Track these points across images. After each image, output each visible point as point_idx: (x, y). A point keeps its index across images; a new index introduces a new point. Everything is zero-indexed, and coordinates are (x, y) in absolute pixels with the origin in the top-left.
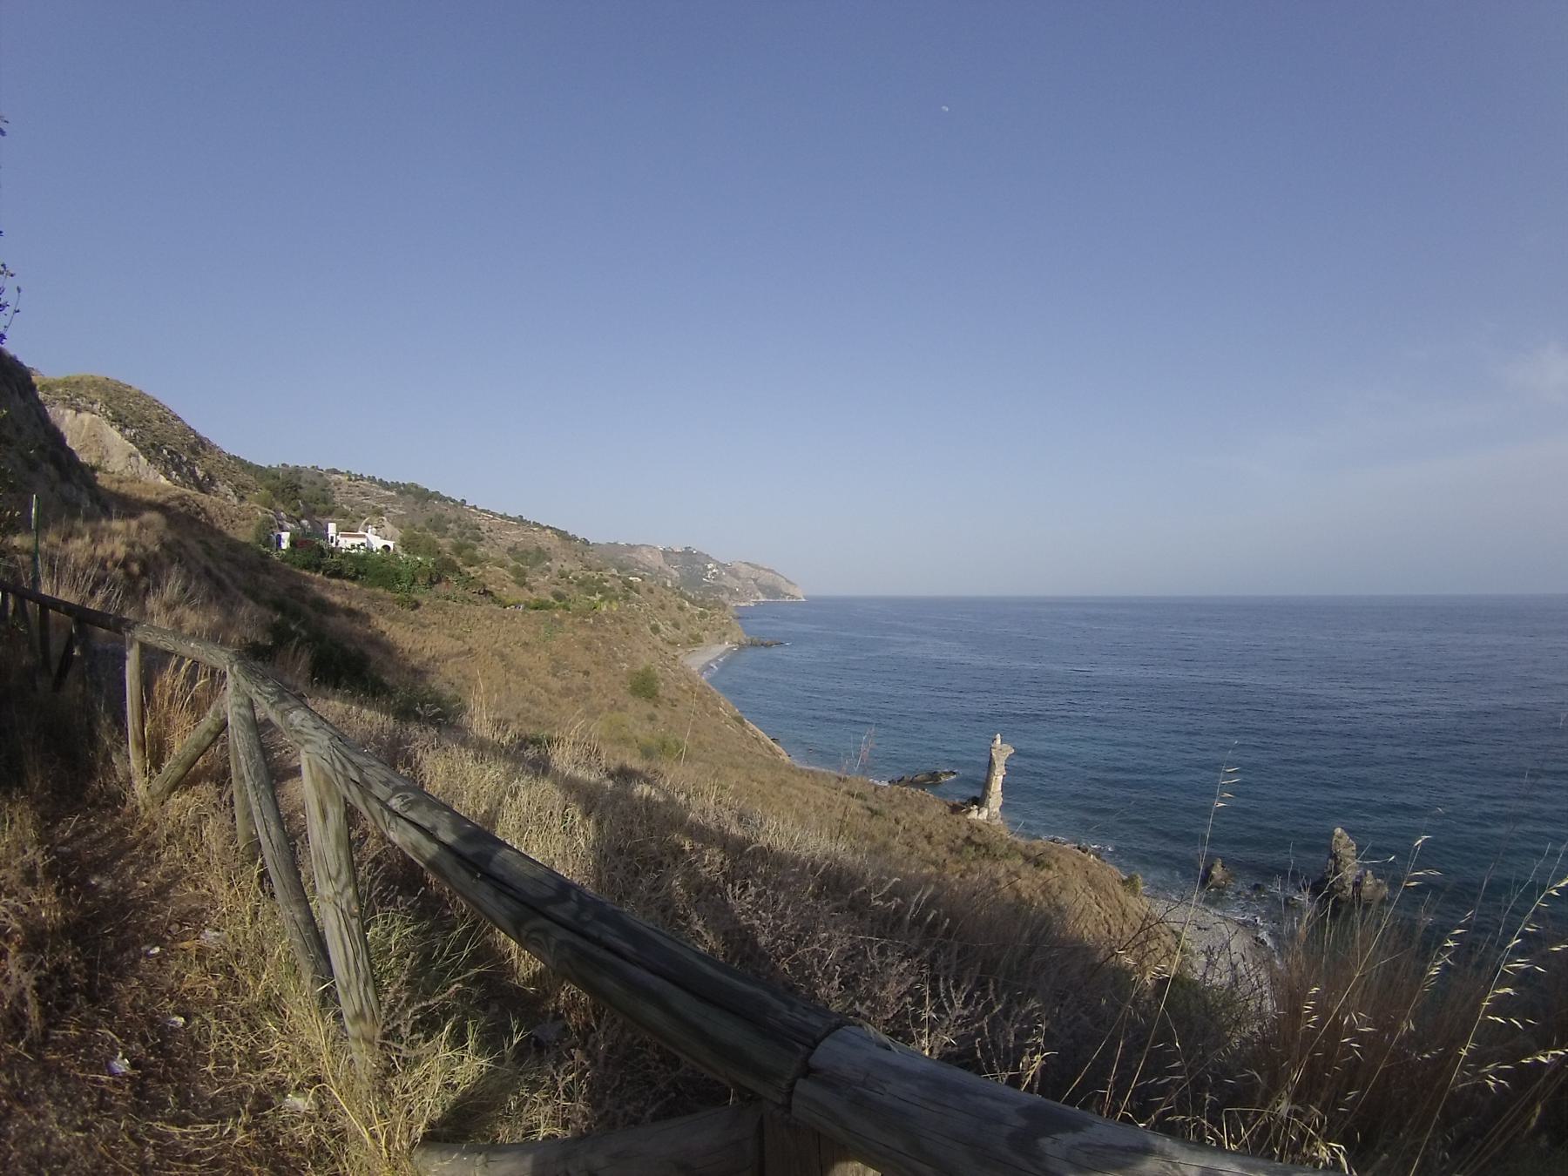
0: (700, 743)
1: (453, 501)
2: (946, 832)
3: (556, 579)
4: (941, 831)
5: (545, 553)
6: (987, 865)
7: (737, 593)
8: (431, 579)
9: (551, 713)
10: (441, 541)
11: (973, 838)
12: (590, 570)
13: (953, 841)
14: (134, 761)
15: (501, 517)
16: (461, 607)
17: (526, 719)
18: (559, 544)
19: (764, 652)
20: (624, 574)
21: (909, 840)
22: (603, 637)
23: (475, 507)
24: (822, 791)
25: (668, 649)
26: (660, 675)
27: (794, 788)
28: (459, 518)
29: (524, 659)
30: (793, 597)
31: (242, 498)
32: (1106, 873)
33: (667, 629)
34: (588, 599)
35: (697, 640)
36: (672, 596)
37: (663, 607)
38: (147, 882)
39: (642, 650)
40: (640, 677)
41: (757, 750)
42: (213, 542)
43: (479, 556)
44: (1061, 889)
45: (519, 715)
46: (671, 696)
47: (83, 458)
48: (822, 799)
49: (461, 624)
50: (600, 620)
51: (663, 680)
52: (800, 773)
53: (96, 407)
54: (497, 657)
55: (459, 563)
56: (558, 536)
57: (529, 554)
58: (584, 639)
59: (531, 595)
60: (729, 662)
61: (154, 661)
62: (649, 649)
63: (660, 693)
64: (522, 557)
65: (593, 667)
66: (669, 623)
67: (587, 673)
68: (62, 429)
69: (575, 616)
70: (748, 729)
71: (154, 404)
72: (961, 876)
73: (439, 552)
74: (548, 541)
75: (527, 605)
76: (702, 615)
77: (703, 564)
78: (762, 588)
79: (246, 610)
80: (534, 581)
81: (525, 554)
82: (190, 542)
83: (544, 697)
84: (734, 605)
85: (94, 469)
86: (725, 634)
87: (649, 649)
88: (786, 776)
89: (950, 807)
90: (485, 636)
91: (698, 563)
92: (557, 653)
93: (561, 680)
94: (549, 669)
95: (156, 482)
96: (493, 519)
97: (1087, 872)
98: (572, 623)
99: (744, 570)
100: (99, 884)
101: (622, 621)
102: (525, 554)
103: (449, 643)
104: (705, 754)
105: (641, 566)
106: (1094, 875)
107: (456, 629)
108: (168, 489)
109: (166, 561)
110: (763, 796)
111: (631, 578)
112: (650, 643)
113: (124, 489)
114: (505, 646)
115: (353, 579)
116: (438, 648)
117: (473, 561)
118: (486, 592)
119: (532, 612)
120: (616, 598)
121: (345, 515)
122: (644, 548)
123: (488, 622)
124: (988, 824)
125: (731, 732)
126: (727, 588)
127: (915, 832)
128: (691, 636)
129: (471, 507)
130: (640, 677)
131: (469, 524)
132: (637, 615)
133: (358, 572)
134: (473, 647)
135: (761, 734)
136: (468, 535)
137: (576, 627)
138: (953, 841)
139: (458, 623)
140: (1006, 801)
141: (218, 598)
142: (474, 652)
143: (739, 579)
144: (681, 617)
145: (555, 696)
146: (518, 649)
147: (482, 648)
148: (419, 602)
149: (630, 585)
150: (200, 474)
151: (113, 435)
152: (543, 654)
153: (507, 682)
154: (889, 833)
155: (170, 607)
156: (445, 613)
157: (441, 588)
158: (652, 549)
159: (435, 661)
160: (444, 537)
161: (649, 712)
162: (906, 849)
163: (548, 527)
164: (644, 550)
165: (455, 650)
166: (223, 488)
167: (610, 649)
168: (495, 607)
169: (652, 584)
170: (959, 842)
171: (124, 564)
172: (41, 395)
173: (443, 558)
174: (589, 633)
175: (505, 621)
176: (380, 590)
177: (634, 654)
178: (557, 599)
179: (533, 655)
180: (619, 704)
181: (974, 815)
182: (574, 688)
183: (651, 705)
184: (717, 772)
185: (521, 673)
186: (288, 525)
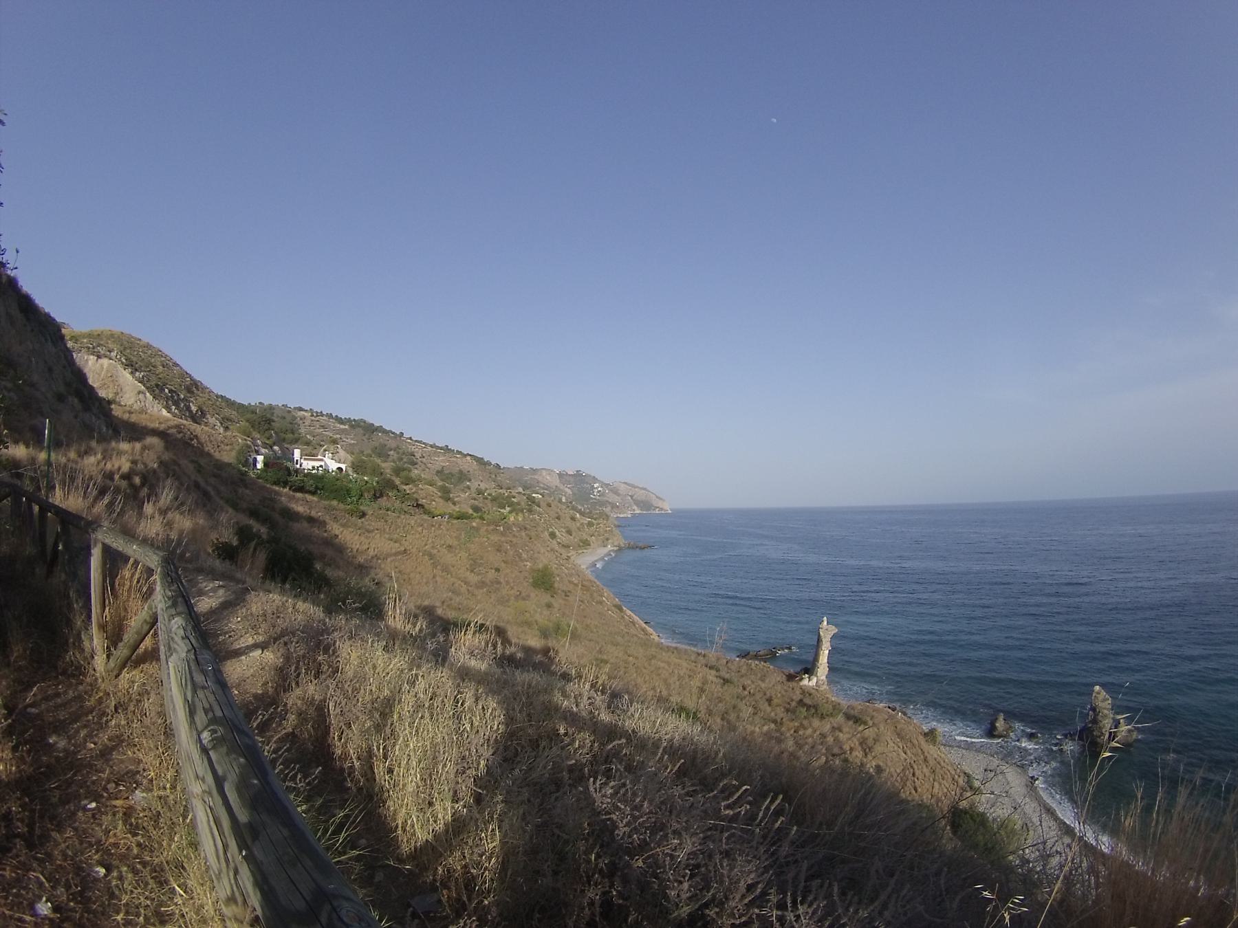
0: (587, 625)
1: (393, 433)
2: (783, 696)
3: (474, 495)
4: (779, 695)
5: (465, 475)
6: (816, 722)
7: (618, 507)
9: (469, 601)
10: (383, 465)
12: (501, 489)
13: (789, 704)
14: (96, 641)
15: (431, 446)
16: (399, 517)
18: (476, 468)
20: (528, 492)
22: (511, 541)
23: (410, 438)
24: (685, 664)
25: (563, 551)
26: (556, 572)
27: (662, 662)
29: (448, 558)
30: (662, 509)
31: (227, 428)
34: (499, 511)
35: (586, 544)
38: (95, 744)
40: (540, 574)
41: (633, 631)
42: (203, 461)
44: (875, 741)
45: (443, 602)
47: (102, 393)
48: (684, 670)
50: (508, 527)
52: (666, 649)
53: (113, 354)
54: (426, 557)
55: (397, 481)
61: (114, 560)
63: (556, 585)
65: (503, 565)
66: (564, 531)
67: (497, 570)
68: (86, 371)
69: (488, 525)
71: (158, 353)
72: (795, 732)
73: (382, 474)
74: (467, 465)
75: (451, 516)
76: (590, 524)
77: (590, 484)
78: (638, 503)
79: (228, 517)
80: (457, 497)
81: (450, 476)
82: (184, 462)
84: (615, 516)
85: (109, 402)
86: (607, 539)
88: (656, 652)
89: (787, 676)
91: (587, 483)
93: (477, 575)
94: (468, 566)
95: (159, 414)
96: (424, 447)
97: (896, 727)
98: (487, 531)
99: (622, 488)
100: (56, 743)
101: (525, 528)
102: (450, 476)
104: (591, 635)
105: (542, 485)
108: (168, 420)
109: (162, 475)
111: (534, 495)
113: (134, 418)
114: (433, 547)
115: (313, 493)
118: (418, 506)
119: (455, 521)
120: (522, 511)
121: (308, 443)
122: (544, 471)
125: (611, 616)
126: (610, 503)
127: (758, 696)
128: (581, 541)
129: (407, 438)
132: (538, 524)
133: (317, 488)
134: (408, 548)
135: (636, 618)
136: (405, 460)
137: (490, 533)
138: (789, 704)
139: (396, 530)
141: (205, 506)
142: (409, 552)
143: (619, 495)
144: (573, 526)
149: (533, 500)
150: (194, 409)
151: (126, 376)
152: (464, 554)
153: (434, 577)
154: (737, 697)
155: (163, 512)
156: (386, 521)
157: (383, 502)
158: (550, 471)
159: (378, 559)
160: (386, 461)
161: (546, 601)
164: (544, 473)
165: (394, 551)
166: (212, 420)
167: (516, 551)
168: (426, 517)
169: (550, 500)
170: (794, 704)
171: (127, 477)
172: (70, 344)
174: (500, 538)
175: (433, 529)
176: (335, 503)
178: (475, 511)
180: (523, 594)
181: (805, 682)
182: (488, 581)
183: (549, 596)
184: (600, 649)
185: (446, 569)
186: (263, 451)
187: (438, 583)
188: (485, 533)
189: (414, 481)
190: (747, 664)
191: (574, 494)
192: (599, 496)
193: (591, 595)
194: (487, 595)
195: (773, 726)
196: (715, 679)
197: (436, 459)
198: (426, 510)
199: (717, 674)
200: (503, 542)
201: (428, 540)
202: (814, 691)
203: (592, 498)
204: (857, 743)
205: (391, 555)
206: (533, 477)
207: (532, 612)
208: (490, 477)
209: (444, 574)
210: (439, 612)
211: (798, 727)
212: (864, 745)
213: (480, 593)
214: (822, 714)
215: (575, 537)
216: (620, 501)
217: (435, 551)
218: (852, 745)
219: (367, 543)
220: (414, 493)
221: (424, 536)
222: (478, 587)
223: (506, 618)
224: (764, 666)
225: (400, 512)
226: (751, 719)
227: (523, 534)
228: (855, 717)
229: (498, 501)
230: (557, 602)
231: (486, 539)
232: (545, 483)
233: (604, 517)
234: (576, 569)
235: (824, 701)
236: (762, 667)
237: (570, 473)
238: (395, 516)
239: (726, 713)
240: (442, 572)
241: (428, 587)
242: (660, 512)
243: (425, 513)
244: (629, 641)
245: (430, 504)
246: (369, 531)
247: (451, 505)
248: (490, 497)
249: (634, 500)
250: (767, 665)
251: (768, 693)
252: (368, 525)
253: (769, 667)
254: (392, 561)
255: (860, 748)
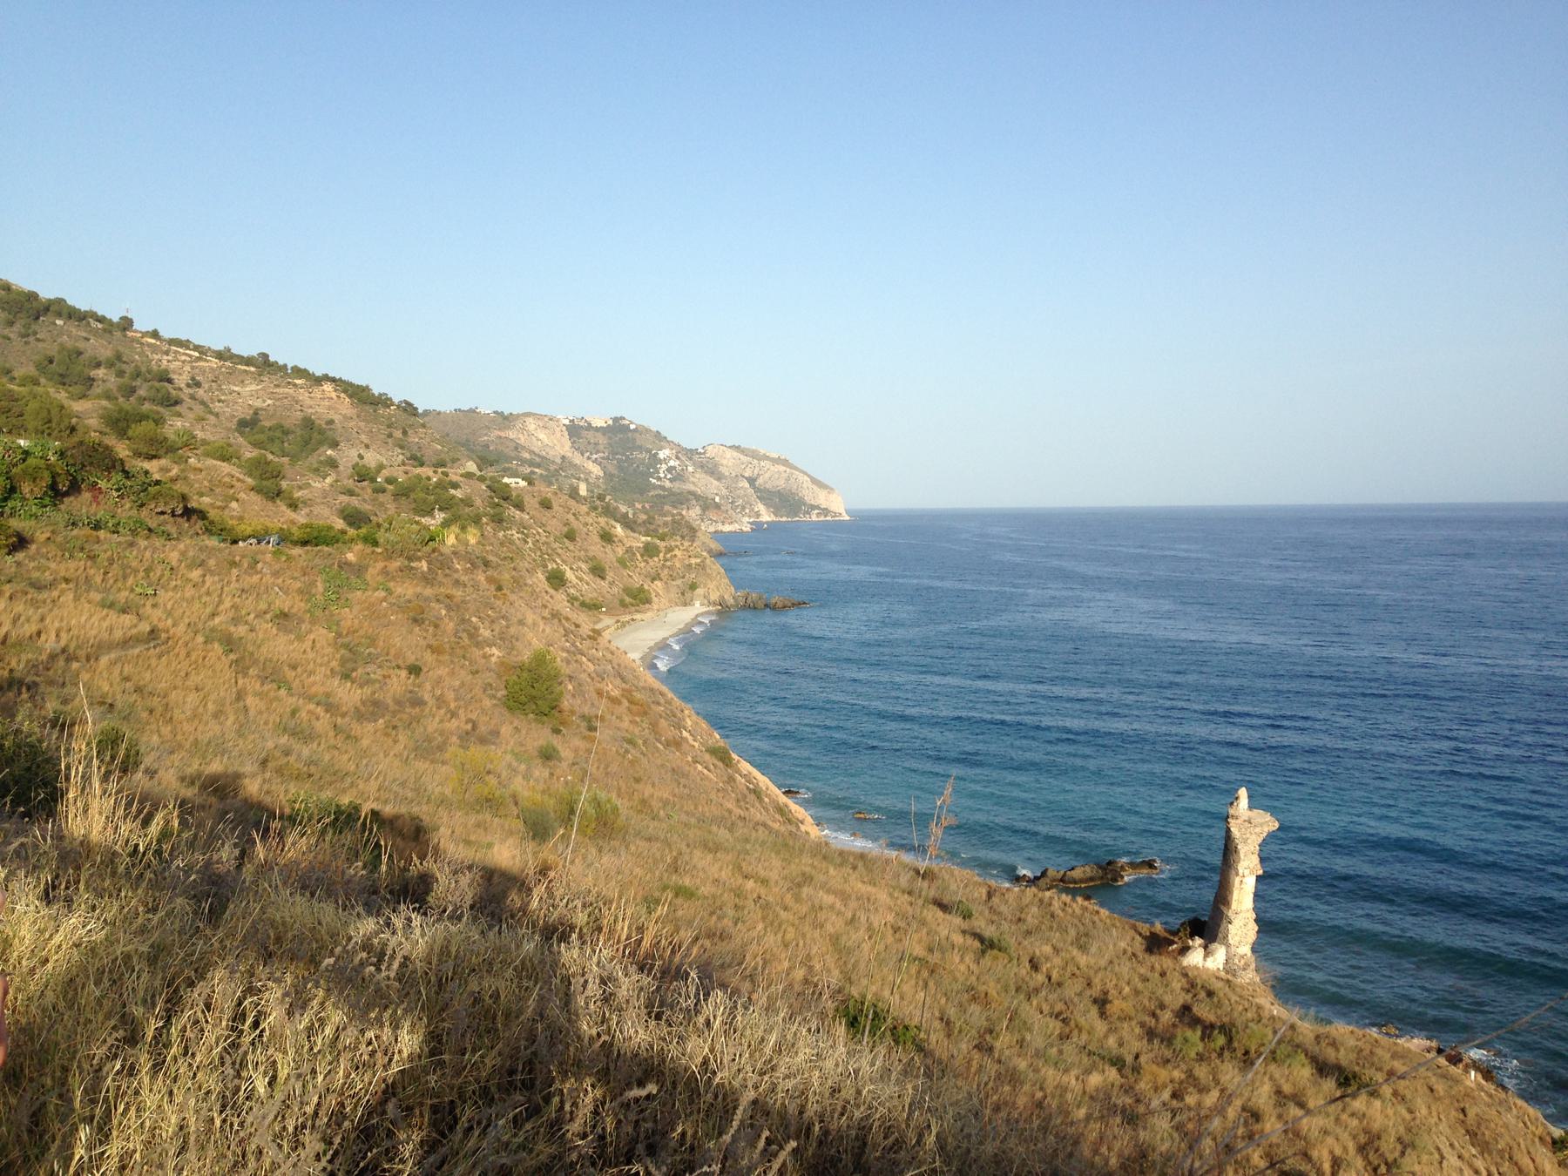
0: (644, 802)
1: (101, 319)
2: (1137, 992)
3: (350, 483)
4: (1127, 989)
5: (321, 432)
6: (1230, 1073)
7: (718, 506)
8: (53, 487)
9: (336, 753)
10: (78, 406)
11: (1195, 1009)
12: (422, 465)
13: (1154, 1015)
15: (220, 355)
16: (131, 544)
17: (279, 771)
18: (351, 412)
19: (769, 618)
21: (1059, 1007)
23: (155, 334)
25: (583, 618)
26: (566, 670)
27: (828, 891)
28: (119, 357)
29: (279, 646)
30: (826, 511)
32: (1510, 1118)
33: (581, 579)
34: (417, 523)
35: (638, 599)
36: (588, 514)
37: (570, 536)
39: (529, 621)
41: (757, 814)
43: (172, 437)
44: (1405, 1145)
45: (264, 763)
46: (586, 710)
49: (130, 581)
50: (442, 563)
51: (571, 678)
52: (838, 860)
54: (216, 645)
55: (122, 450)
56: (350, 397)
57: (286, 432)
58: (410, 601)
59: (293, 515)
60: (692, 645)
62: (543, 618)
63: (566, 704)
64: (272, 440)
65: (429, 657)
66: (583, 566)
67: (415, 670)
69: (389, 555)
70: (738, 771)
72: (1174, 1095)
73: (73, 429)
74: (325, 405)
75: (284, 538)
76: (650, 551)
77: (650, 451)
78: (766, 496)
80: (300, 488)
81: (278, 434)
83: (323, 723)
84: (712, 529)
86: (693, 587)
87: (543, 618)
88: (812, 865)
89: (1145, 938)
90: (190, 601)
91: (640, 448)
92: (353, 632)
93: (361, 687)
94: (334, 664)
96: (199, 359)
97: (1463, 1110)
98: (384, 572)
99: (729, 462)
101: (486, 564)
102: (278, 434)
103: (104, 619)
104: (652, 824)
105: (526, 455)
106: (1480, 1120)
107: (119, 590)
110: (767, 906)
111: (506, 480)
112: (545, 606)
114: (236, 621)
116: (75, 632)
117: (157, 448)
118: (188, 513)
119: (297, 551)
120: (476, 521)
122: (530, 420)
123: (195, 574)
124: (1228, 981)
126: (697, 497)
127: (1072, 989)
128: (627, 591)
129: (145, 334)
130: (525, 675)
131: (144, 369)
132: (519, 551)
134: (161, 625)
135: (763, 781)
136: (142, 392)
137: (393, 579)
138: (1154, 1015)
139: (125, 577)
140: (1213, 804)
142: (164, 635)
144: (608, 555)
145: (347, 719)
146: (266, 627)
147: (182, 628)
148: (28, 535)
149: (503, 495)
152: (322, 635)
153: (240, 696)
154: (1018, 989)
156: (92, 558)
157: (81, 504)
158: (547, 421)
159: (69, 660)
160: (84, 396)
161: (542, 742)
162: (1055, 1026)
163: (326, 378)
164: (531, 425)
165: (118, 635)
167: (463, 621)
168: (213, 542)
169: (548, 491)
170: (1167, 1017)
173: (81, 443)
174: (419, 590)
175: (235, 571)
177: (512, 630)
178: (351, 524)
179: (300, 638)
180: (483, 729)
181: (1195, 957)
184: (676, 859)
185: (273, 675)
187: (252, 712)
188: (380, 579)
189: (171, 450)
190: (1041, 901)
191: (609, 476)
192: (671, 480)
193: (654, 726)
194: (387, 735)
195: (1112, 1074)
196: (958, 939)
197: (236, 389)
198: (212, 523)
199: (965, 925)
200: (427, 599)
201: (220, 602)
202: (1220, 985)
203: (655, 487)
204: (1351, 1146)
205: (111, 646)
206: (503, 435)
207: (504, 774)
208: (390, 436)
209: (266, 688)
210: (253, 787)
211: (1181, 1082)
212: (1372, 1156)
213: (367, 732)
214: (1247, 1053)
215: (612, 584)
216: (724, 492)
217: (242, 630)
218: (1338, 1152)
219: (36, 617)
220: (174, 480)
221: (208, 593)
222: (360, 716)
223: (437, 790)
224: (1085, 909)
225: (134, 532)
226: (1055, 1050)
227: (481, 578)
228: (1338, 1068)
229: (413, 496)
230: (568, 747)
231: (383, 594)
232: (536, 450)
233: (685, 531)
234: (615, 662)
235: (1249, 1015)
236: (1078, 911)
237: (599, 422)
238: (120, 543)
239: (991, 1032)
240: (262, 684)
241: (220, 724)
242: (822, 518)
243: (208, 531)
244: (747, 840)
245: (223, 508)
246: (39, 587)
247: (284, 508)
248: (391, 487)
249: (757, 490)
250: (1092, 905)
251: (1097, 981)
252: (38, 568)
253: (1098, 912)
254: (113, 663)
255: (1359, 1162)
